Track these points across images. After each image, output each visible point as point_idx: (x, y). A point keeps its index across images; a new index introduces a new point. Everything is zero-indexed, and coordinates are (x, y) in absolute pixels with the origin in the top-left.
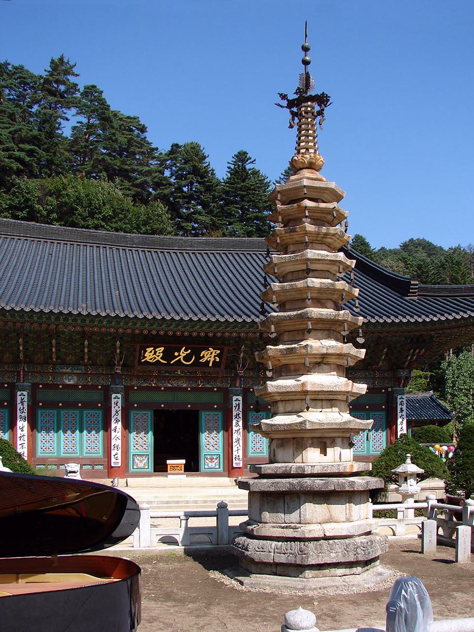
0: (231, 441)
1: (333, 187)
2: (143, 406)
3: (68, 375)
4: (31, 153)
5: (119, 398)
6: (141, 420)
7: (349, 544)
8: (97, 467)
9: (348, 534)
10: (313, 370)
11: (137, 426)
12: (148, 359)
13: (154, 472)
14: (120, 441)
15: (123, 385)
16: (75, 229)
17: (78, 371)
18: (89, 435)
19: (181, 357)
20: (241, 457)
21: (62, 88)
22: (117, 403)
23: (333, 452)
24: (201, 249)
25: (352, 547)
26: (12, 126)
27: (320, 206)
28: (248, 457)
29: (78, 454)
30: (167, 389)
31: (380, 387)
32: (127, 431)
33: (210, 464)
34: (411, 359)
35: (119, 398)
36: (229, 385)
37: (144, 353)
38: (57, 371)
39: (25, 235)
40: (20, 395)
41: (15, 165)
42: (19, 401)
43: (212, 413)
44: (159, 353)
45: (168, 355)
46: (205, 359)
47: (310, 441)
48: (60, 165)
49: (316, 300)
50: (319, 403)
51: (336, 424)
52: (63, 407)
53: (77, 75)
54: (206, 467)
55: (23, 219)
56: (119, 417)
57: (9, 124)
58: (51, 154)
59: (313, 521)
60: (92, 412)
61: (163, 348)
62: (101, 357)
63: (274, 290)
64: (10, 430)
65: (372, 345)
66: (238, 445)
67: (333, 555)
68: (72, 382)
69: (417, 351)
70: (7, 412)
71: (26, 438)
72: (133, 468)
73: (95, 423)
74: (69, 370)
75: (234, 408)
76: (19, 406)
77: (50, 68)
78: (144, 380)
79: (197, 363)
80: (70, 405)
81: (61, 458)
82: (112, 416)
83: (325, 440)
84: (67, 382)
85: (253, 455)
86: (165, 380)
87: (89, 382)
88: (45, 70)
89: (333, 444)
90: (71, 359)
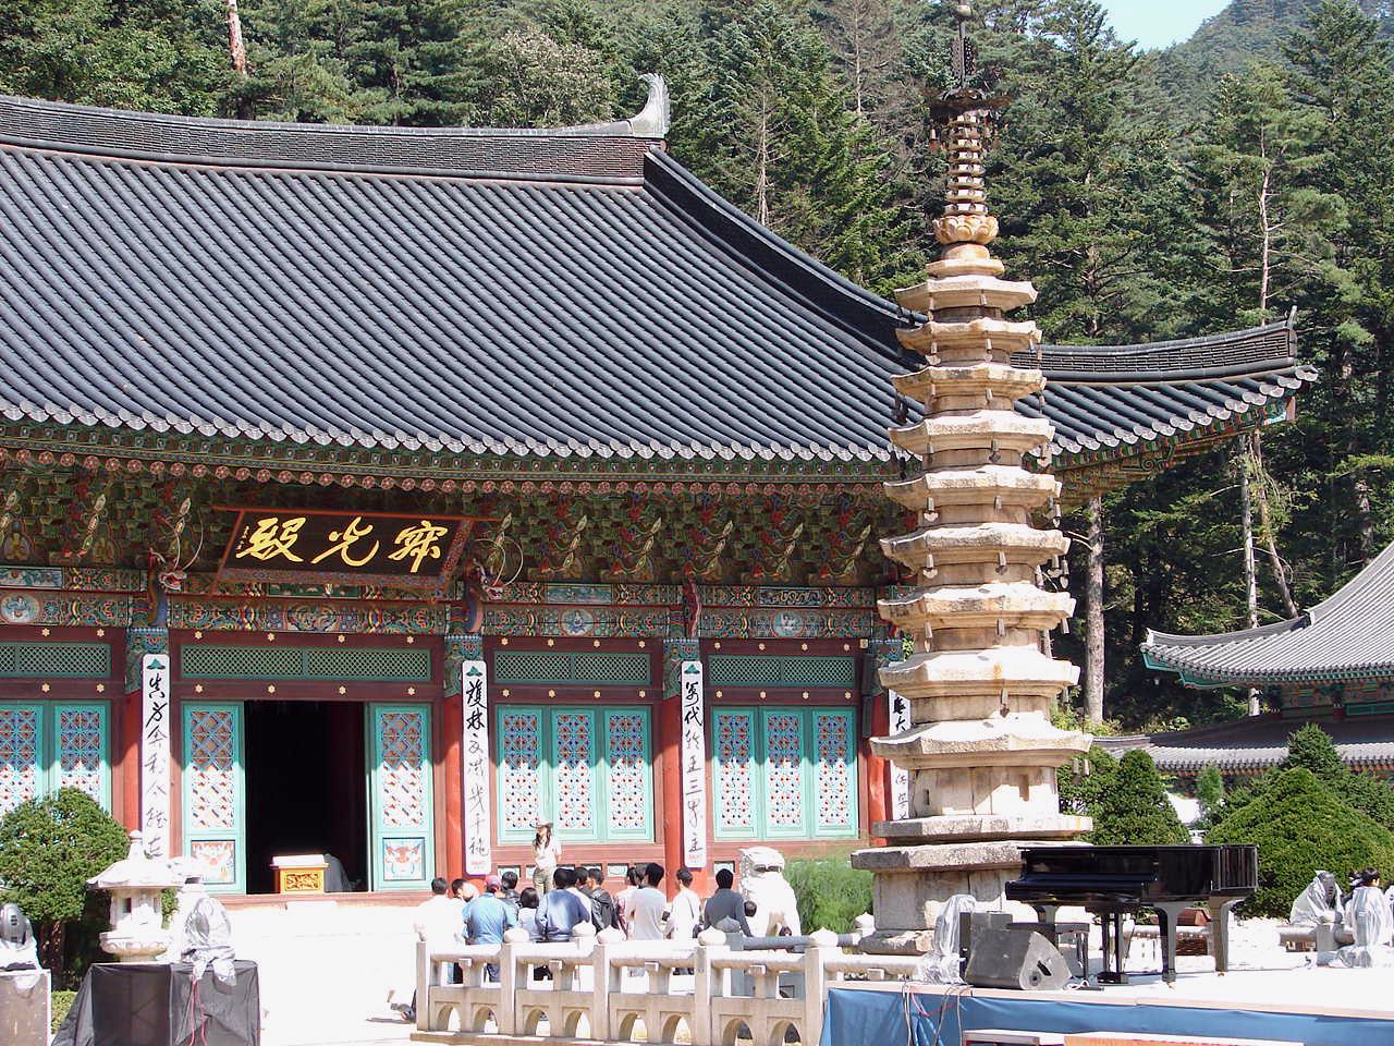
0: (457, 795)
2: (218, 691)
5: (163, 667)
6: (212, 735)
11: (203, 753)
12: (254, 551)
17: (45, 585)
19: (344, 546)
22: (157, 683)
24: (245, 161)
30: (284, 638)
31: (840, 636)
33: (398, 866)
35: (163, 667)
37: (250, 534)
43: (401, 711)
44: (291, 533)
45: (310, 542)
46: (403, 553)
47: (1004, 774)
52: (810, 704)
61: (304, 520)
62: (103, 540)
63: (931, 487)
65: (825, 512)
66: (478, 809)
68: (24, 619)
70: (423, 716)
73: (88, 745)
75: (466, 697)
78: (225, 613)
79: (381, 565)
82: (145, 723)
83: (1026, 771)
84: (12, 618)
90: (17, 547)
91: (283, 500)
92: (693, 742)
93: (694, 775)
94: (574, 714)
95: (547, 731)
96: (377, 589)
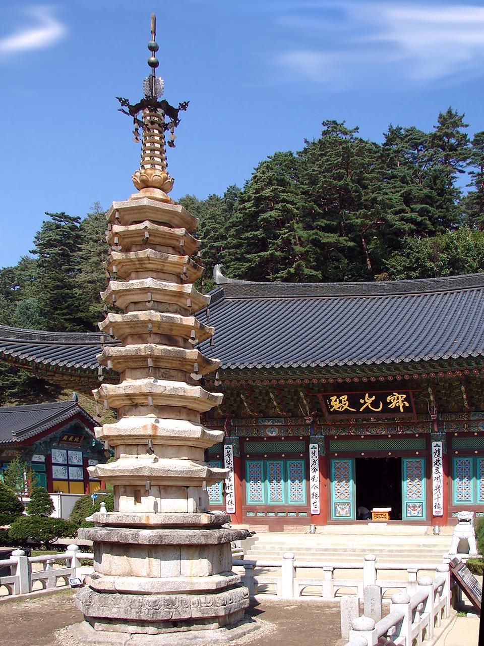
1: (145, 204)
2: (343, 455)
3: (271, 427)
4: (422, 212)
5: (316, 448)
7: (134, 601)
8: (259, 514)
9: (139, 590)
10: (129, 413)
12: (336, 408)
13: (357, 519)
14: (319, 489)
15: (322, 434)
16: (326, 283)
17: (279, 424)
18: (293, 484)
20: (441, 505)
21: (452, 141)
23: (148, 502)
24: (454, 288)
25: (137, 603)
26: (402, 189)
27: (129, 229)
28: (247, 505)
29: (284, 502)
30: (367, 437)
32: (450, 477)
33: (413, 513)
35: (316, 448)
36: (430, 430)
37: (330, 403)
38: (260, 425)
39: (280, 296)
40: (226, 448)
41: (407, 227)
42: (225, 454)
43: (414, 460)
44: (344, 401)
48: (454, 220)
49: (138, 335)
50: (135, 449)
51: (128, 471)
52: (267, 459)
53: (467, 126)
54: (409, 515)
55: (417, 278)
56: (317, 467)
58: (444, 210)
59: (112, 573)
60: (295, 462)
64: (474, 478)
67: (115, 610)
68: (274, 434)
71: (233, 487)
72: (335, 516)
74: (270, 423)
75: (433, 455)
76: (226, 458)
77: (439, 123)
80: (275, 456)
81: (268, 506)
83: (138, 488)
84: (270, 435)
85: (459, 503)
86: (363, 428)
87: (290, 433)
88: (434, 127)
89: (147, 493)
90: (273, 413)
91: (339, 389)
94: (275, 462)
95: (285, 468)
96: (400, 418)
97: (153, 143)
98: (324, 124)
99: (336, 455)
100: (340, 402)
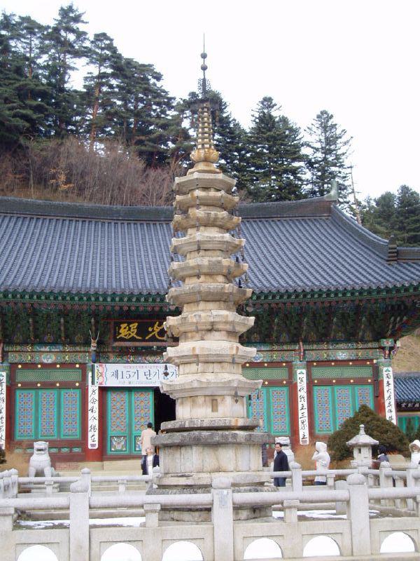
12: (122, 335)
14: (97, 421)
19: (156, 333)
29: (56, 437)
34: (393, 327)
52: (60, 388)
57: (15, 79)
61: (137, 324)
68: (50, 361)
69: (398, 319)
74: (47, 349)
83: (216, 398)
92: (302, 399)
93: (303, 411)
97: (203, 123)
98: (325, 121)
99: (39, 385)
100: (130, 329)
